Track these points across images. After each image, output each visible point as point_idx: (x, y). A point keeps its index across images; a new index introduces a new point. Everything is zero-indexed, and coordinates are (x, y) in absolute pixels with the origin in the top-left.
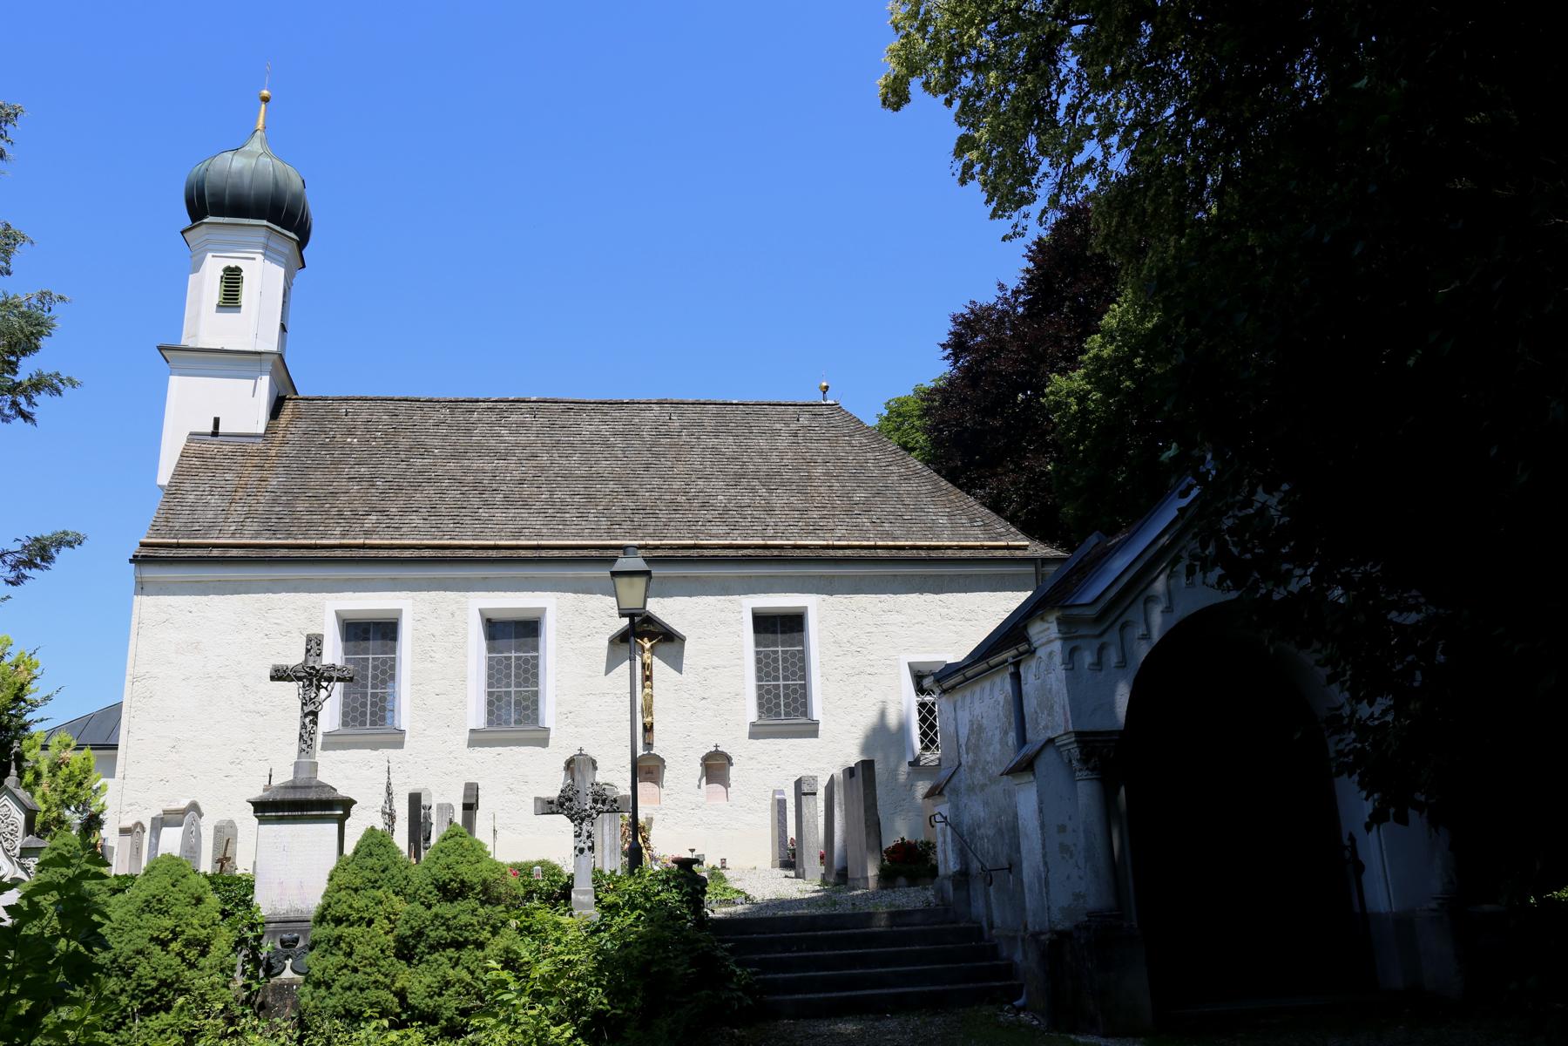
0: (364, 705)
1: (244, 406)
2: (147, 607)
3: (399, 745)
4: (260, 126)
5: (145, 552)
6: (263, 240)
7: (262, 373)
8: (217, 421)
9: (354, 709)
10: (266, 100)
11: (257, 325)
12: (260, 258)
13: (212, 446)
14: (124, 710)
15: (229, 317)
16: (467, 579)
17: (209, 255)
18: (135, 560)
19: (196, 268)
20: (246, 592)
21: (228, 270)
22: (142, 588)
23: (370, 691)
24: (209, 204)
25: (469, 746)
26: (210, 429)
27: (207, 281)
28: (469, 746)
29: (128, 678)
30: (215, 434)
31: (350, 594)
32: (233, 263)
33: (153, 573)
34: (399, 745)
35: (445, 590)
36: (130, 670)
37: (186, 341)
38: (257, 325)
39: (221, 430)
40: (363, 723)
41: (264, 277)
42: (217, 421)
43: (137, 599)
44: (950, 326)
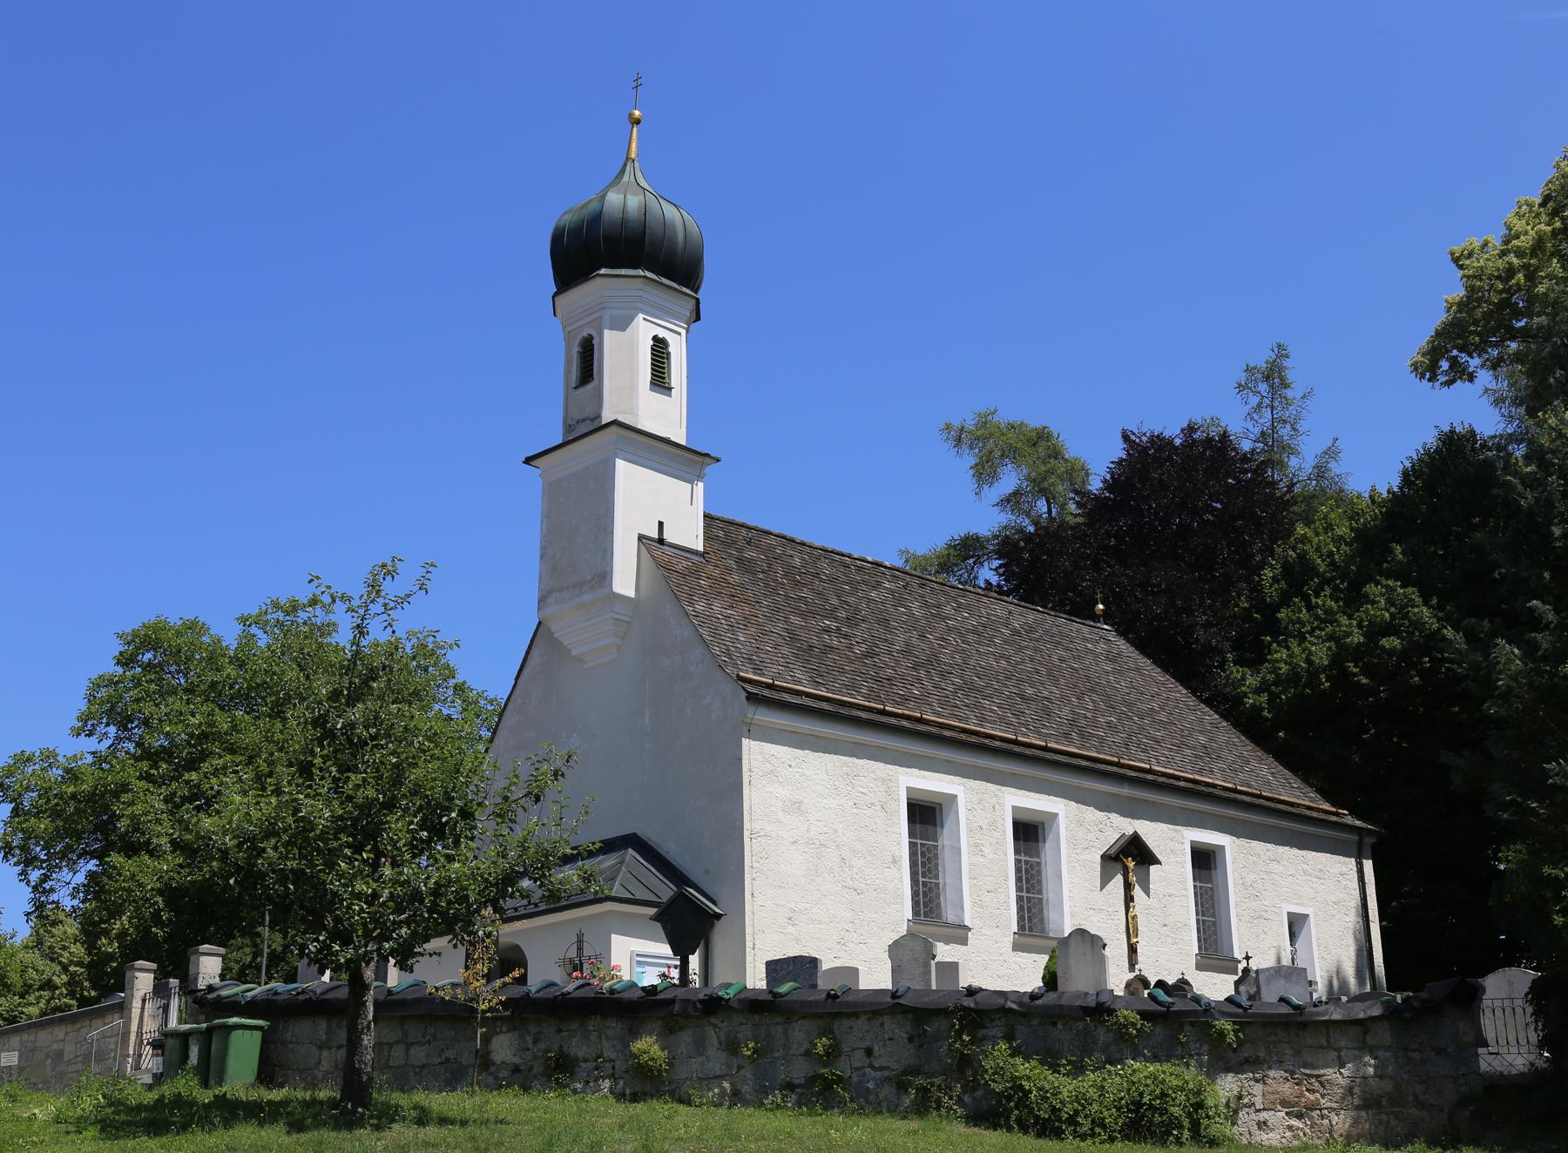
10: (638, 122)
31: (915, 771)
32: (662, 333)
33: (764, 716)
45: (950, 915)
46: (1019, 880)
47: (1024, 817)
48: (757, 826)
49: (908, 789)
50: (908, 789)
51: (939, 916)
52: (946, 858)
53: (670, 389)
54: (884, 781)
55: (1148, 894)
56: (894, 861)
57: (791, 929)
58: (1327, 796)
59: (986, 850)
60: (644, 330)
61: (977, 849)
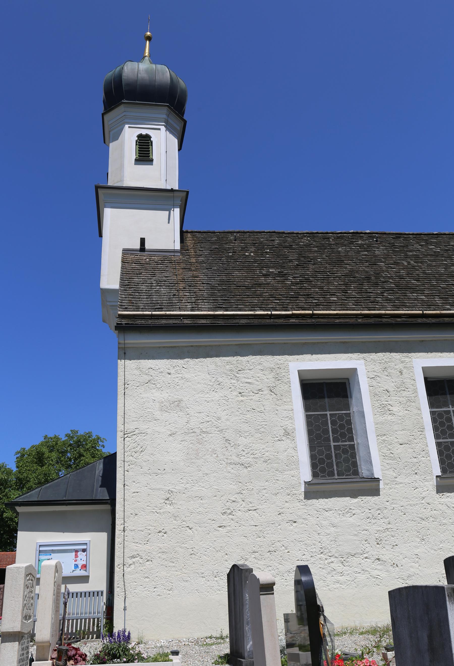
0: (329, 457)
1: (162, 230)
2: (130, 370)
3: (375, 492)
4: (147, 54)
5: (124, 322)
6: (165, 116)
7: (174, 206)
8: (143, 241)
9: (322, 461)
10: (149, 38)
11: (164, 171)
12: (163, 128)
13: (138, 260)
14: (119, 463)
15: (144, 168)
16: (407, 342)
17: (127, 126)
18: (119, 328)
19: (116, 137)
20: (217, 356)
21: (140, 136)
22: (125, 353)
23: (332, 444)
24: (121, 95)
25: (438, 491)
26: (138, 246)
27: (130, 135)
28: (438, 491)
29: (120, 434)
30: (143, 248)
31: (308, 356)
32: (144, 132)
33: (134, 340)
34: (375, 492)
35: (391, 352)
36: (120, 427)
37: (110, 183)
38: (164, 171)
39: (147, 247)
40: (331, 474)
41: (164, 141)
42: (143, 241)
43: (121, 363)
44: (42, 439)
45: (364, 471)
46: (435, 429)
47: (431, 375)
48: (130, 427)
49: (300, 372)
50: (300, 372)
51: (356, 473)
52: (356, 419)
53: (152, 160)
54: (272, 370)
55: (304, 570)
56: (287, 434)
57: (169, 508)
58: (322, 652)
59: (395, 409)
60: (130, 135)
61: (384, 409)
